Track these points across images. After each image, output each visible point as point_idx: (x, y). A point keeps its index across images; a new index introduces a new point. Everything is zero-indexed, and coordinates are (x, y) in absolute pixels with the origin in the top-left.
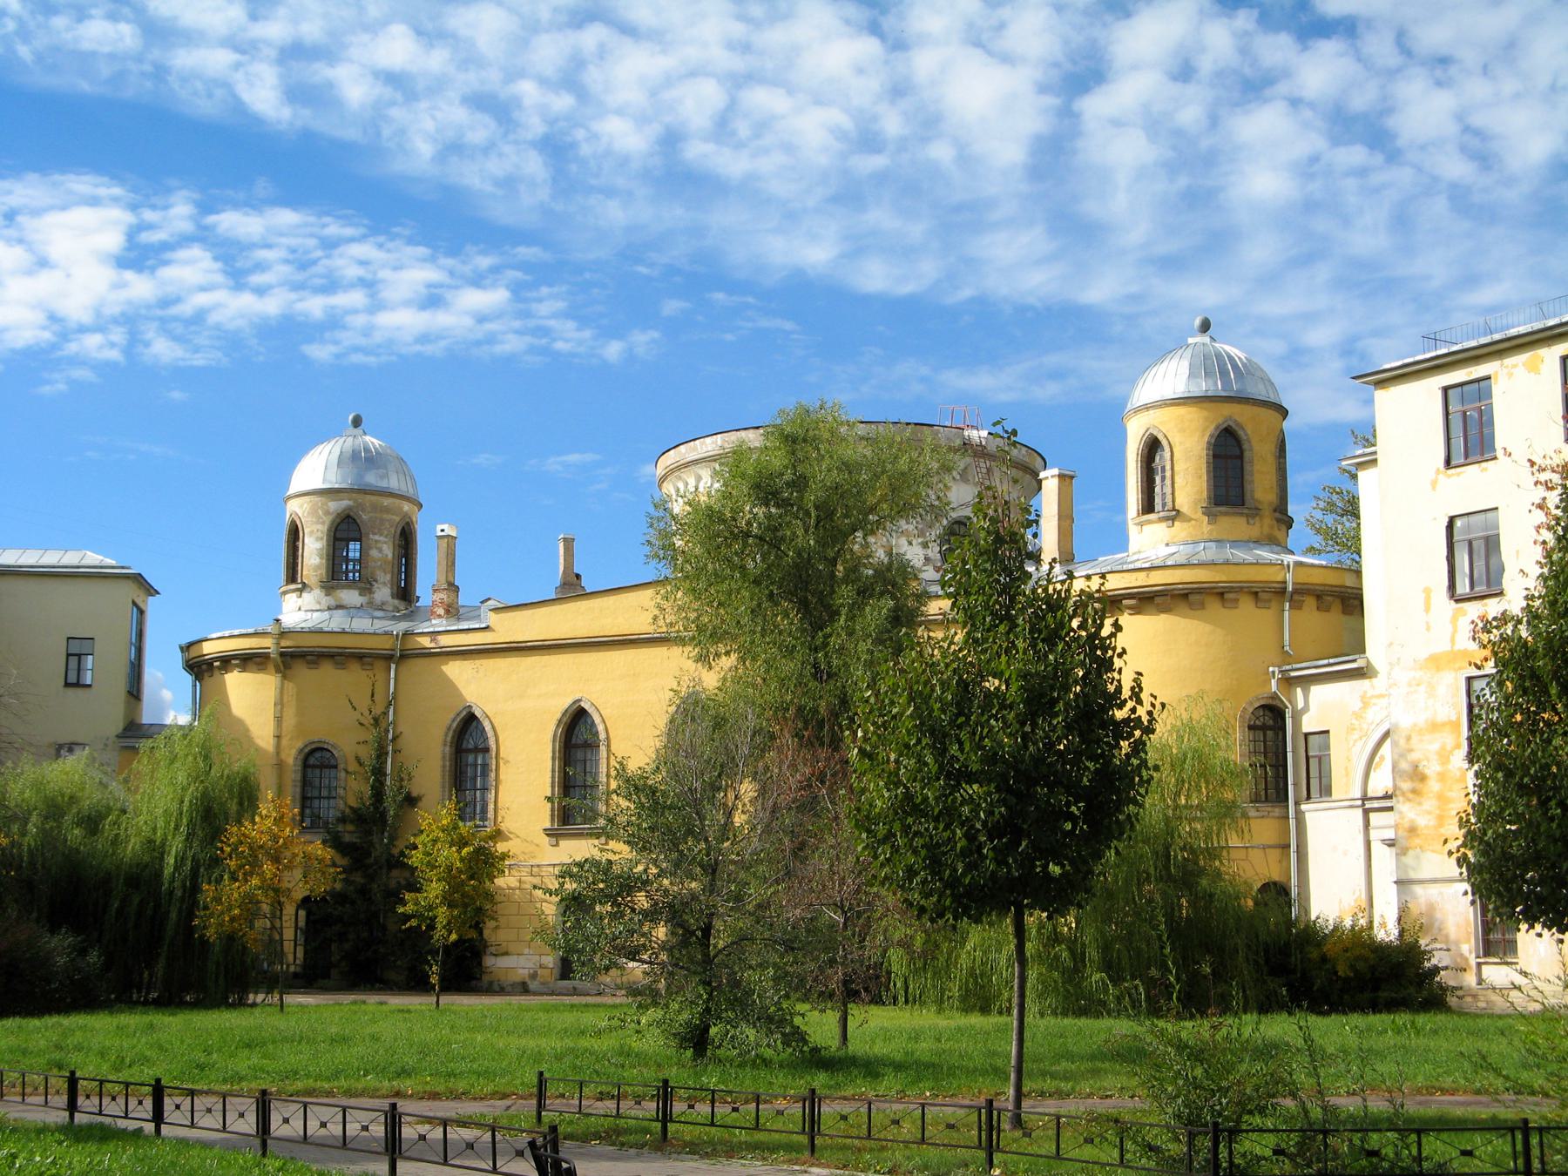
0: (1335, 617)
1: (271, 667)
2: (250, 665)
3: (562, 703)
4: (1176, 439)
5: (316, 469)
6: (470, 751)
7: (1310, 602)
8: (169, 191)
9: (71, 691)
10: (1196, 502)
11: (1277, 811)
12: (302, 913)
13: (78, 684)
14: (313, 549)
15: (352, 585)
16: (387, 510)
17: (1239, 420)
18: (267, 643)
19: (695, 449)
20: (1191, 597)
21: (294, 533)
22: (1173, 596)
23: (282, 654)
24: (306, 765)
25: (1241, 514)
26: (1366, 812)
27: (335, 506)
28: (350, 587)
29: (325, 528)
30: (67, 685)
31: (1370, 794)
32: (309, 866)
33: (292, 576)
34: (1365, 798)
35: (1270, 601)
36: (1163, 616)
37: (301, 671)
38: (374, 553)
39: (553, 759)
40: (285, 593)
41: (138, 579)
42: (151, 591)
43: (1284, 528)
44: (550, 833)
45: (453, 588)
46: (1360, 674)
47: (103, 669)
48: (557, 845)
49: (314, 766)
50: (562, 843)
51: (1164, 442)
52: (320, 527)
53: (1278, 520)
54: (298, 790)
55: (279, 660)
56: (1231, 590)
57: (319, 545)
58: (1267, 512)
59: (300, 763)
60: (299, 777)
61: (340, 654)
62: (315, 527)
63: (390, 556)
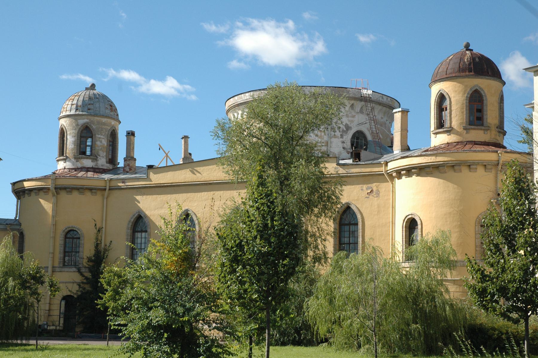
4: (452, 95)
6: (138, 232)
8: (75, 145)
10: (461, 124)
12: (63, 303)
14: (70, 140)
15: (88, 157)
16: (104, 124)
18: (49, 184)
19: (241, 98)
20: (456, 168)
24: (66, 237)
25: (481, 129)
28: (87, 158)
29: (77, 132)
32: (69, 282)
35: (491, 169)
36: (429, 178)
37: (63, 195)
38: (98, 143)
40: (58, 161)
43: (502, 135)
49: (69, 238)
51: (447, 97)
52: (74, 131)
53: (499, 132)
54: (62, 248)
55: (54, 191)
57: (73, 139)
58: (493, 128)
59: (63, 236)
60: (62, 242)
61: (82, 188)
62: (72, 131)
63: (106, 145)
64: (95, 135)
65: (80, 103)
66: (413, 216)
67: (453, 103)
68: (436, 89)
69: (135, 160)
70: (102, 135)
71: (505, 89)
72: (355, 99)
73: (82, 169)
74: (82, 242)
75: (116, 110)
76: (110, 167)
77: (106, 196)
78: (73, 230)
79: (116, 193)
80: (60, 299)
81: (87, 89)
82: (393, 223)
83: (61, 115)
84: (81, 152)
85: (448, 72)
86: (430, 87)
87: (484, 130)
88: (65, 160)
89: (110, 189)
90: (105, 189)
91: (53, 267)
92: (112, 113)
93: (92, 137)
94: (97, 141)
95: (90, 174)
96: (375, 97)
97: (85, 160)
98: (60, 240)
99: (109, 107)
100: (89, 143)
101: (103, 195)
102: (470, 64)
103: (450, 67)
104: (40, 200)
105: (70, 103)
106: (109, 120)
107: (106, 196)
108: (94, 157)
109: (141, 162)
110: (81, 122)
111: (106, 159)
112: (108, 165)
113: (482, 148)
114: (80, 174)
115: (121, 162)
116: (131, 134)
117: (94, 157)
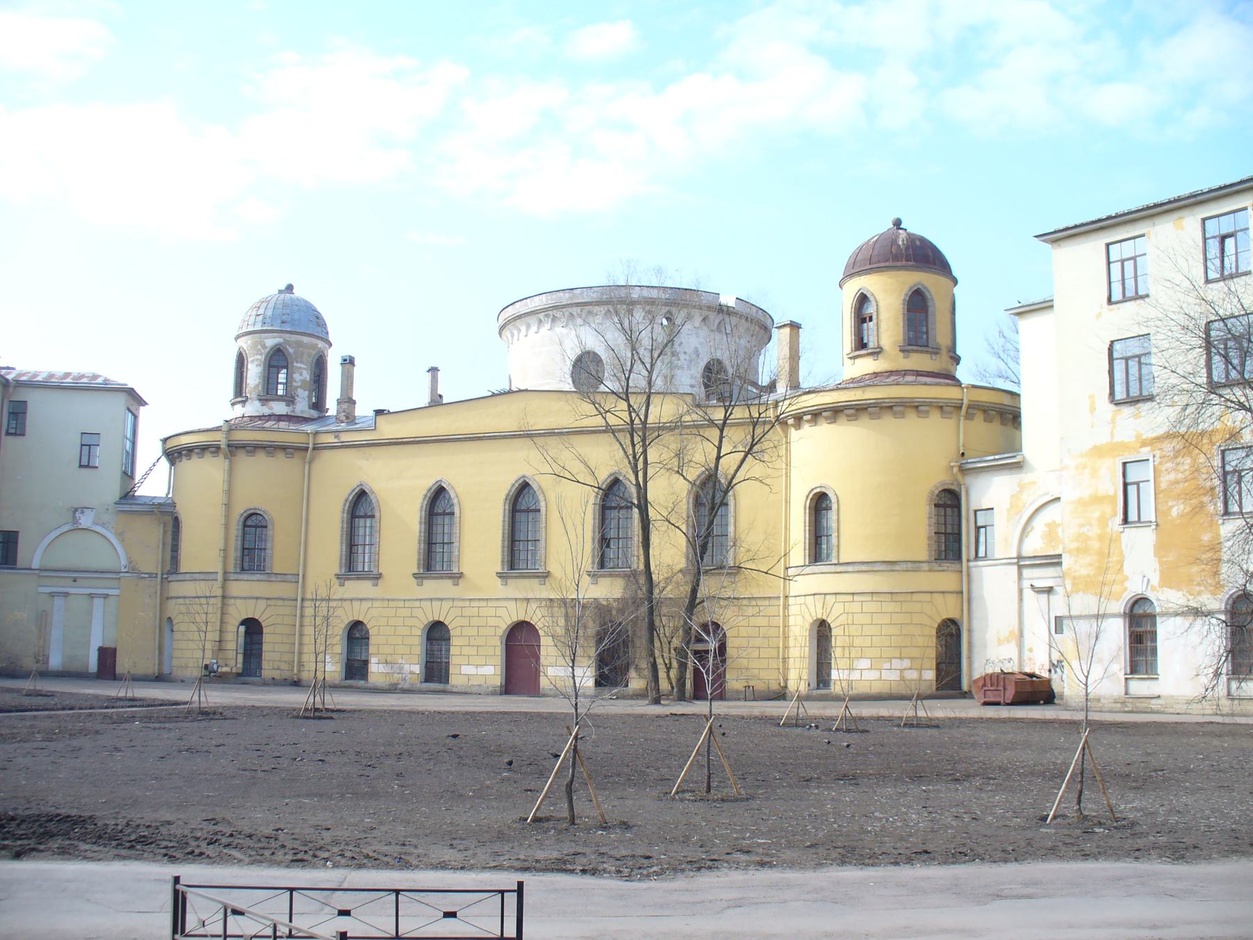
0: (996, 427)
1: (221, 456)
3: (425, 484)
4: (880, 297)
7: (979, 417)
9: (83, 470)
11: (956, 566)
12: (242, 629)
13: (88, 466)
14: (254, 374)
15: (280, 399)
18: (221, 438)
22: (882, 408)
24: (245, 526)
25: (927, 352)
26: (1020, 567)
30: (81, 466)
31: (1025, 554)
34: (1020, 557)
38: (296, 376)
39: (593, 556)
40: (233, 404)
41: (131, 393)
42: (142, 402)
44: (501, 576)
46: (1018, 466)
47: (107, 457)
51: (871, 298)
56: (924, 404)
58: (944, 351)
60: (240, 533)
65: (269, 313)
66: (823, 490)
67: (882, 310)
69: (354, 402)
71: (956, 290)
72: (709, 308)
73: (270, 417)
74: (270, 533)
76: (314, 414)
79: (327, 455)
80: (237, 624)
81: (280, 292)
82: (788, 502)
84: (268, 394)
87: (931, 353)
88: (244, 402)
90: (306, 449)
91: (225, 573)
92: (319, 329)
93: (286, 367)
95: (282, 425)
96: (741, 308)
98: (235, 530)
99: (313, 319)
100: (282, 377)
101: (304, 458)
102: (907, 249)
103: (875, 253)
106: (314, 341)
108: (290, 399)
109: (363, 409)
110: (271, 342)
113: (929, 380)
115: (331, 406)
116: (349, 362)
117: (290, 399)
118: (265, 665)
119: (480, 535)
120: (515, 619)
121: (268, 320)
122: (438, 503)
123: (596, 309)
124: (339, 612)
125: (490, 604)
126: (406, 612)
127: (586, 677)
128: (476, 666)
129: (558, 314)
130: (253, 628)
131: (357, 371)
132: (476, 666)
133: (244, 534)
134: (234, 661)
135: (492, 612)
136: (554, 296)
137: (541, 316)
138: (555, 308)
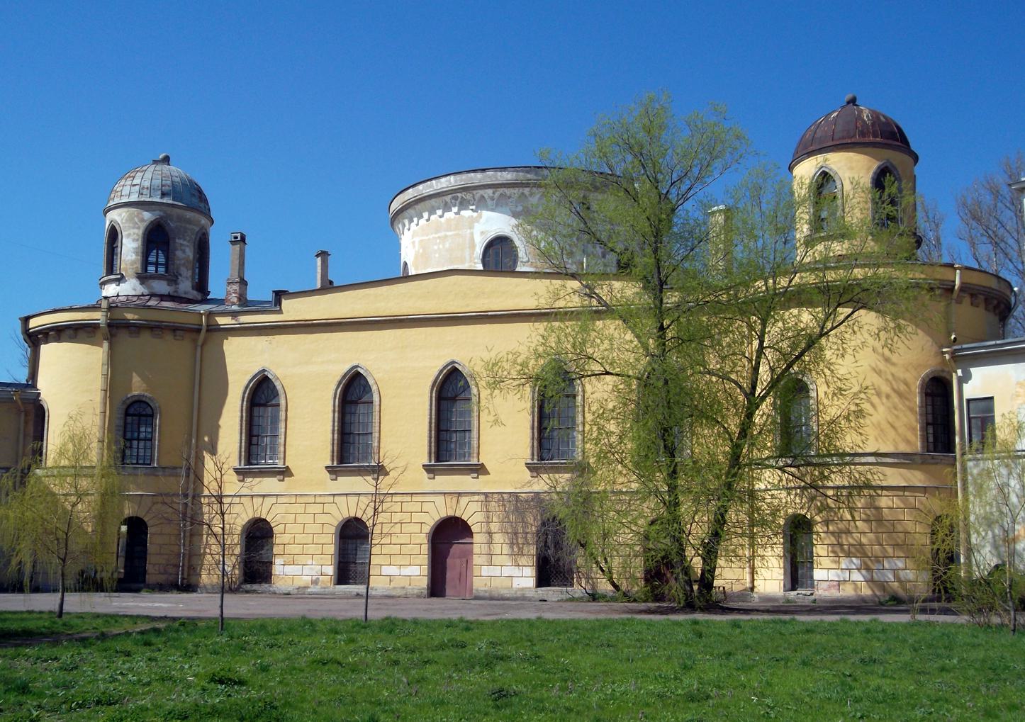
2: (81, 334)
3: (341, 369)
5: (139, 183)
14: (130, 248)
16: (189, 221)
17: (894, 163)
18: (98, 317)
19: (432, 186)
21: (114, 235)
23: (109, 325)
24: (127, 414)
27: (148, 216)
29: (140, 232)
33: (110, 268)
37: (127, 342)
45: (243, 283)
48: (336, 479)
50: (286, 479)
60: (122, 423)
61: (158, 327)
62: (132, 231)
63: (191, 257)
64: (174, 238)
68: (806, 170)
70: (185, 240)
71: (918, 170)
75: (206, 202)
77: (200, 342)
78: (147, 404)
83: (111, 203)
85: (836, 137)
86: (791, 169)
89: (208, 331)
90: (199, 331)
92: (202, 205)
94: (177, 250)
97: (157, 281)
99: (197, 193)
101: (195, 341)
102: (873, 125)
104: (134, 374)
105: (129, 182)
107: (200, 342)
108: (172, 278)
111: (192, 282)
112: (195, 292)
114: (153, 303)
117: (172, 278)
118: (149, 567)
119: (403, 428)
120: (444, 515)
121: (145, 191)
122: (354, 392)
123: (508, 191)
124: (236, 509)
125: (415, 498)
126: (318, 508)
127: (524, 578)
128: (399, 567)
129: (468, 196)
130: (137, 527)
131: (248, 249)
132: (399, 567)
133: (125, 424)
134: (113, 565)
135: (417, 507)
136: (464, 176)
137: (448, 198)
138: (465, 189)
